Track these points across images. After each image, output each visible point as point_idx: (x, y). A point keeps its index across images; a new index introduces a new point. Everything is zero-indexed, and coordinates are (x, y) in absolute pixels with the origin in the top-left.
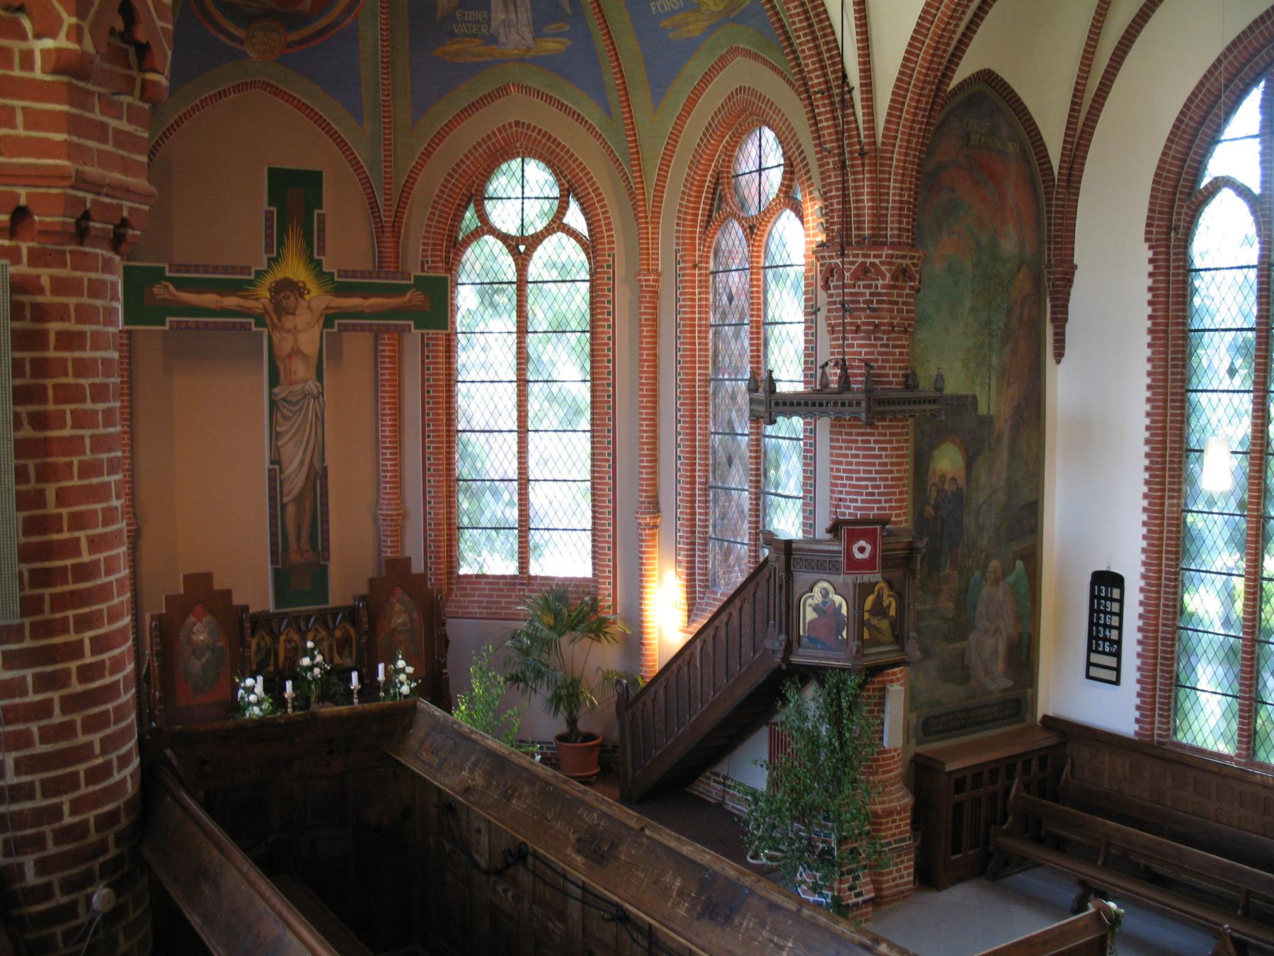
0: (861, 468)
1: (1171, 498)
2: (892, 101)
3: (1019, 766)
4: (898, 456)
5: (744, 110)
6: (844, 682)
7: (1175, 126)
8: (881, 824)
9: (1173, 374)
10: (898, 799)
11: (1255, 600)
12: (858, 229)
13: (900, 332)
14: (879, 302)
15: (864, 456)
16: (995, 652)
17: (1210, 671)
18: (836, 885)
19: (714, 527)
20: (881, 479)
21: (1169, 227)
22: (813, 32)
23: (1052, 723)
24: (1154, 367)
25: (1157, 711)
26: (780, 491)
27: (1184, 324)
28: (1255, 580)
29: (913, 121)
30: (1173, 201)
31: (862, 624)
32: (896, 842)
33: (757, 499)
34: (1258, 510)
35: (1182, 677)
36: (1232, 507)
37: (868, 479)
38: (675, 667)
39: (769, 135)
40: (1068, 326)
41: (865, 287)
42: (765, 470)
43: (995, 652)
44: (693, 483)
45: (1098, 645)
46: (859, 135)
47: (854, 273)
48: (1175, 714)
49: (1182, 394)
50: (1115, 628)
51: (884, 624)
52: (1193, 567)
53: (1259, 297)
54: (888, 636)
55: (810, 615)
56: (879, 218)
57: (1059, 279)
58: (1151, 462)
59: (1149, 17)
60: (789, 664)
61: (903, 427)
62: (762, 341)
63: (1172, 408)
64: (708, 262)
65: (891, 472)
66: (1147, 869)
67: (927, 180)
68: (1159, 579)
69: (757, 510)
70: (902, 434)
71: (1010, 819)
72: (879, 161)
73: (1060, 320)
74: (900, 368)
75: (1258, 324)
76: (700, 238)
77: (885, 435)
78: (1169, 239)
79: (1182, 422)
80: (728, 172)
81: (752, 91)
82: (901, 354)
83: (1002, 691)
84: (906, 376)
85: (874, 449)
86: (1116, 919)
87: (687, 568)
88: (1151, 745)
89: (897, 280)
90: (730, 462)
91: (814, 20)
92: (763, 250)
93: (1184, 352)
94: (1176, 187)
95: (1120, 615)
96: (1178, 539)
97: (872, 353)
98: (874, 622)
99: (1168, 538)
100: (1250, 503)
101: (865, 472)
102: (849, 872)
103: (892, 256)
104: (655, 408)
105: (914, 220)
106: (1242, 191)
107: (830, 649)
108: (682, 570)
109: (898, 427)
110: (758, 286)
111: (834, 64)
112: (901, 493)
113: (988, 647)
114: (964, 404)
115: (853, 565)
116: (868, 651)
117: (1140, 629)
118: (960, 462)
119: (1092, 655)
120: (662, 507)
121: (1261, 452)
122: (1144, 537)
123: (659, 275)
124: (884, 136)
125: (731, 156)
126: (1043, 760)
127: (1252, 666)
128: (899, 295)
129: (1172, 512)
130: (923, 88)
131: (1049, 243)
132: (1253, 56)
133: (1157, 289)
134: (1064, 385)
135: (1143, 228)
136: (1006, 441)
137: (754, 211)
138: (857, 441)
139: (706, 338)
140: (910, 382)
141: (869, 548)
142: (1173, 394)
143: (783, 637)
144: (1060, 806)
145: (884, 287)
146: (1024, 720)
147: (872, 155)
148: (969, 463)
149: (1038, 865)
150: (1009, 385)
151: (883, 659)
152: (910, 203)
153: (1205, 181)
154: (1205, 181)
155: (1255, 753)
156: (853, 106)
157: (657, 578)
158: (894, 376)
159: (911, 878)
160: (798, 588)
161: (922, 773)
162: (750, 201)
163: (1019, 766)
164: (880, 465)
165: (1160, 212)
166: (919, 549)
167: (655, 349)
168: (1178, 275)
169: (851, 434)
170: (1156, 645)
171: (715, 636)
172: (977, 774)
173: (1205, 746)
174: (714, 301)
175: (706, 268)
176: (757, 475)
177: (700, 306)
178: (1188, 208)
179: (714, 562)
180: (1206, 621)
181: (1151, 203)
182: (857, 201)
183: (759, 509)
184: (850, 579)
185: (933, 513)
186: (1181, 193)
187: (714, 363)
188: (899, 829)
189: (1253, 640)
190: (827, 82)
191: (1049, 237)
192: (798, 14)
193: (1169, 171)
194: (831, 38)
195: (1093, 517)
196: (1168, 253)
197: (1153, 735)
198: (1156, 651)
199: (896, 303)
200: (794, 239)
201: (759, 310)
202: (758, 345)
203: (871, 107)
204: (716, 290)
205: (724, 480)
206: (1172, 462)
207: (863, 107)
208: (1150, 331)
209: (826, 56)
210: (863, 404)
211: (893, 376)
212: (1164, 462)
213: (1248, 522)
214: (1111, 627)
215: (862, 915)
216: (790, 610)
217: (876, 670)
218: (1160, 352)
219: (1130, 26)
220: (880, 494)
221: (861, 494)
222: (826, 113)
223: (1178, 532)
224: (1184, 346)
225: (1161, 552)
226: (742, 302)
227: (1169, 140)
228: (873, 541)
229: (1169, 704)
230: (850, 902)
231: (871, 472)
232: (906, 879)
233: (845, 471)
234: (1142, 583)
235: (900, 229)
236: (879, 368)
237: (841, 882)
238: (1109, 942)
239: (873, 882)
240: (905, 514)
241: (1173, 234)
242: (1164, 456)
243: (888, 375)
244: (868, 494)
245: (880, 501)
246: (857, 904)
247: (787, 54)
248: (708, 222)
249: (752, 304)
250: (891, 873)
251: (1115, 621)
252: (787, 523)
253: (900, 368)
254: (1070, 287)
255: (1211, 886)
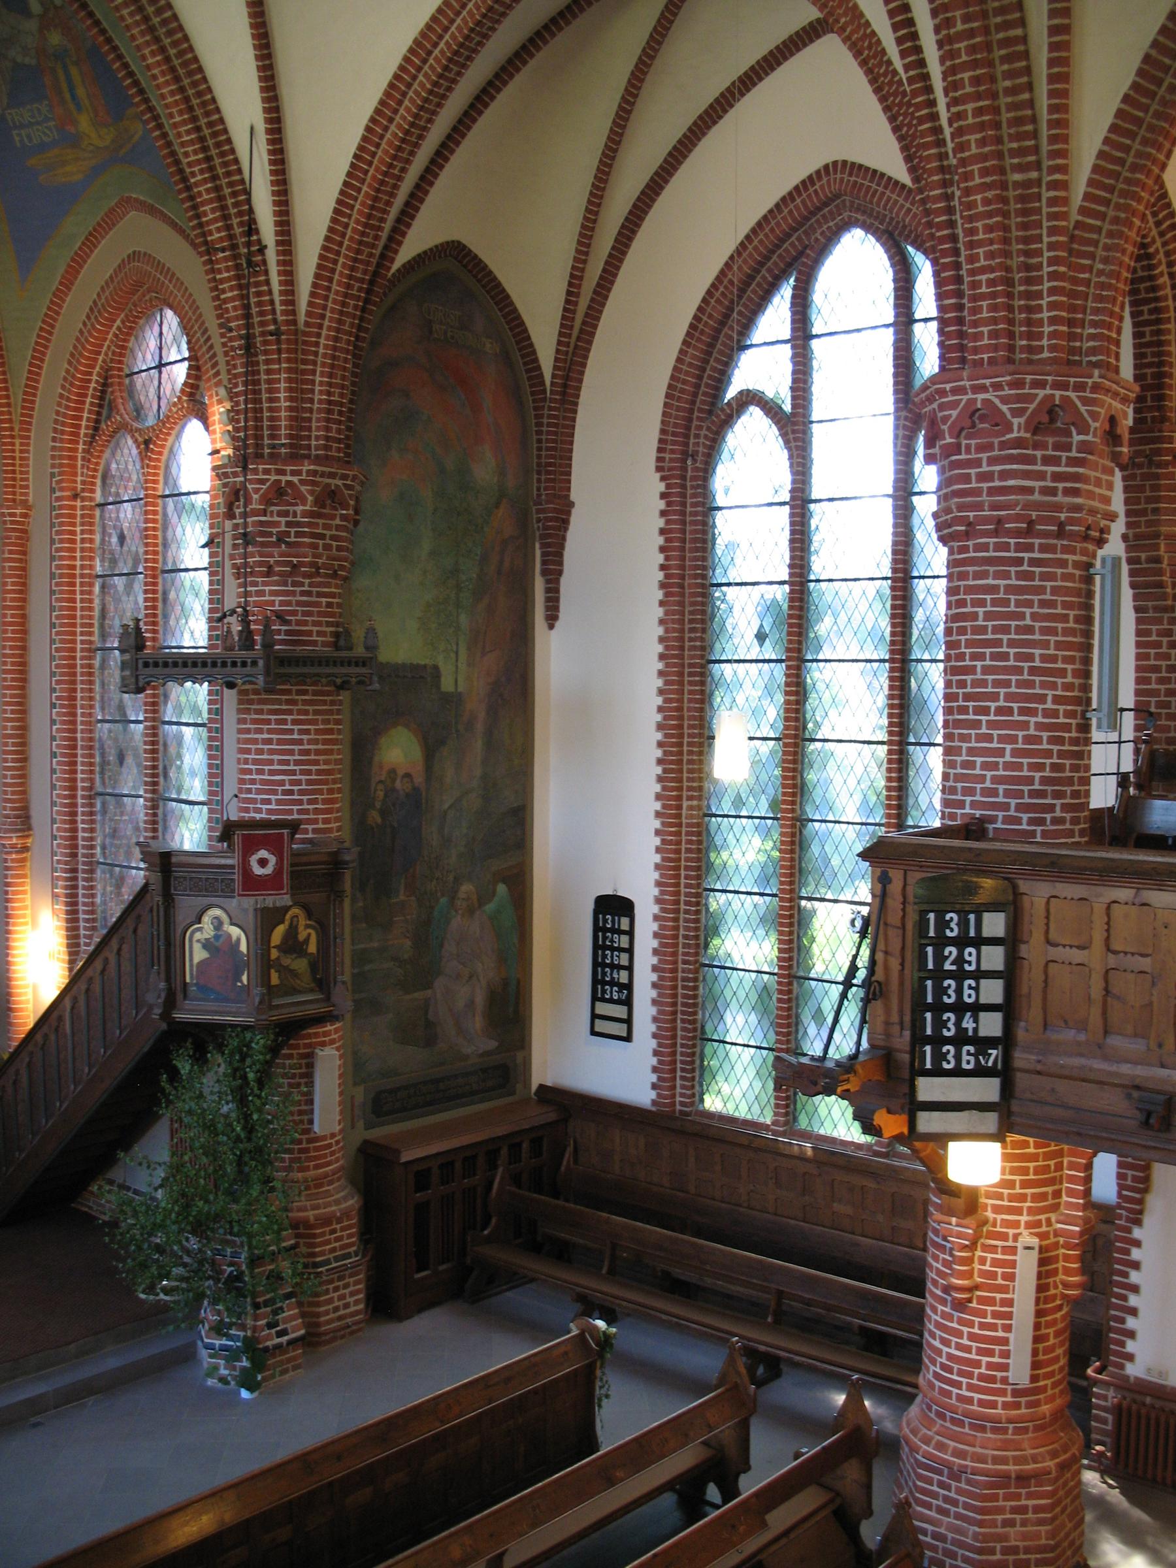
0: (276, 757)
1: (690, 798)
2: (319, 266)
3: (504, 1151)
4: (325, 742)
5: (139, 284)
6: (248, 1046)
7: (692, 326)
8: (314, 1236)
9: (691, 640)
10: (337, 1202)
11: (791, 925)
12: (272, 437)
13: (327, 576)
14: (298, 534)
15: (279, 742)
16: (471, 1004)
17: (740, 1019)
18: (250, 1322)
19: (104, 848)
20: (303, 772)
21: (685, 454)
22: (211, 169)
23: (552, 1096)
24: (667, 631)
25: (679, 1073)
26: (184, 797)
27: (704, 577)
28: (791, 900)
29: (346, 295)
30: (690, 420)
31: (266, 964)
32: (337, 1259)
33: (155, 807)
34: (793, 811)
35: (709, 1028)
36: (763, 809)
37: (287, 774)
38: (39, 1037)
39: (170, 316)
40: (564, 581)
41: (280, 514)
42: (165, 768)
43: (471, 1004)
44: (73, 788)
45: (604, 992)
46: (274, 311)
47: (263, 496)
48: (702, 1076)
49: (703, 666)
50: (624, 968)
51: (300, 965)
52: (718, 886)
53: (792, 541)
54: (306, 981)
55: (199, 954)
56: (299, 422)
57: (551, 519)
58: (665, 753)
59: (662, 188)
60: (172, 1023)
61: (333, 703)
62: (160, 596)
63: (691, 683)
64: (93, 491)
65: (316, 762)
66: (666, 1274)
67: (370, 382)
68: (677, 902)
69: (155, 822)
70: (331, 712)
71: (494, 1220)
72: (300, 347)
73: (553, 575)
74: (328, 624)
75: (791, 575)
76: (83, 459)
77: (306, 713)
78: (684, 469)
79: (702, 701)
80: (120, 370)
81: (148, 258)
82: (329, 605)
83: (482, 1055)
84: (337, 635)
85: (291, 731)
86: (605, 1341)
87: (67, 904)
88: (671, 1116)
89: (323, 506)
90: (121, 758)
91: (214, 152)
92: (161, 472)
93: (704, 612)
94: (693, 403)
95: (630, 951)
96: (699, 851)
97: (289, 603)
98: (287, 961)
99: (688, 851)
100: (784, 802)
101: (281, 762)
102: (266, 1304)
103: (314, 473)
104: (23, 688)
105: (349, 429)
106: (771, 409)
107: (227, 1000)
108: (61, 907)
109: (324, 703)
110: (155, 521)
111: (240, 214)
112: (331, 791)
113: (461, 997)
114: (420, 677)
115: (252, 884)
116: (275, 1002)
117: (655, 969)
118: (417, 753)
119: (598, 1004)
120: (35, 822)
121: (796, 736)
122: (658, 850)
123: (29, 508)
124: (309, 314)
125: (124, 348)
126: (536, 1143)
127: (789, 1009)
128: (327, 527)
129: (692, 817)
130: (358, 252)
131: (539, 473)
132: (782, 241)
133: (670, 531)
134: (557, 656)
135: (653, 454)
136: (480, 727)
137: (151, 421)
138: (268, 722)
139: (90, 593)
140: (342, 643)
141: (273, 860)
142: (691, 665)
143: (162, 985)
144: (560, 1202)
145: (305, 514)
146: (512, 1093)
147: (294, 340)
148: (429, 755)
149: (532, 1280)
150: (483, 654)
151: (298, 1012)
152: (342, 404)
153: (731, 393)
154: (731, 393)
155: (795, 1119)
156: (266, 272)
157: (29, 919)
158: (319, 633)
159: (361, 1306)
160: (182, 916)
161: (372, 1167)
162: (147, 405)
163: (504, 1151)
164: (301, 752)
165: (674, 434)
166: (347, 863)
167: (22, 608)
168: (696, 514)
169: (261, 712)
170: (675, 987)
171: (88, 990)
172: (446, 1163)
173: (737, 1114)
174: (103, 541)
175: (91, 499)
176: (154, 775)
177: (83, 550)
178: (708, 429)
179: (103, 894)
180: (736, 957)
181: (663, 422)
182: (270, 400)
183: (158, 819)
184: (249, 903)
185: (379, 820)
186: (700, 410)
187: (102, 626)
188: (341, 1241)
189: (789, 976)
190: (231, 237)
191: (539, 465)
192: (192, 142)
193: (684, 382)
194: (237, 178)
195: (595, 827)
196: (684, 487)
197: (674, 1104)
198: (675, 996)
199: (322, 537)
200: (197, 456)
201: (156, 553)
202: (155, 600)
203: (290, 273)
204: (104, 527)
205: (116, 782)
206: (690, 753)
207: (280, 273)
208: (663, 585)
209: (230, 201)
210: (261, 663)
211: (319, 638)
212: (681, 753)
213: (782, 826)
214: (620, 967)
215: (289, 1360)
216: (171, 949)
217: (289, 1030)
218: (674, 613)
219: (639, 199)
220: (301, 792)
221: (275, 792)
222: (229, 279)
223: (700, 842)
224: (703, 604)
225: (678, 868)
226: (135, 545)
227: (685, 342)
228: (277, 851)
229: (693, 1062)
230: (269, 1343)
231: (287, 762)
232: (353, 1309)
233: (255, 762)
234: (656, 909)
235: (327, 438)
236: (298, 623)
237: (256, 1318)
238: (598, 1373)
239: (303, 1315)
240: (337, 820)
241: (689, 462)
242: (680, 745)
243: (310, 633)
244: (285, 792)
245: (300, 802)
246: (279, 1347)
247: (183, 201)
248: (93, 436)
249: (147, 545)
250: (331, 1301)
251: (624, 959)
252: (191, 834)
253: (328, 624)
254: (566, 529)
255: (741, 1289)
